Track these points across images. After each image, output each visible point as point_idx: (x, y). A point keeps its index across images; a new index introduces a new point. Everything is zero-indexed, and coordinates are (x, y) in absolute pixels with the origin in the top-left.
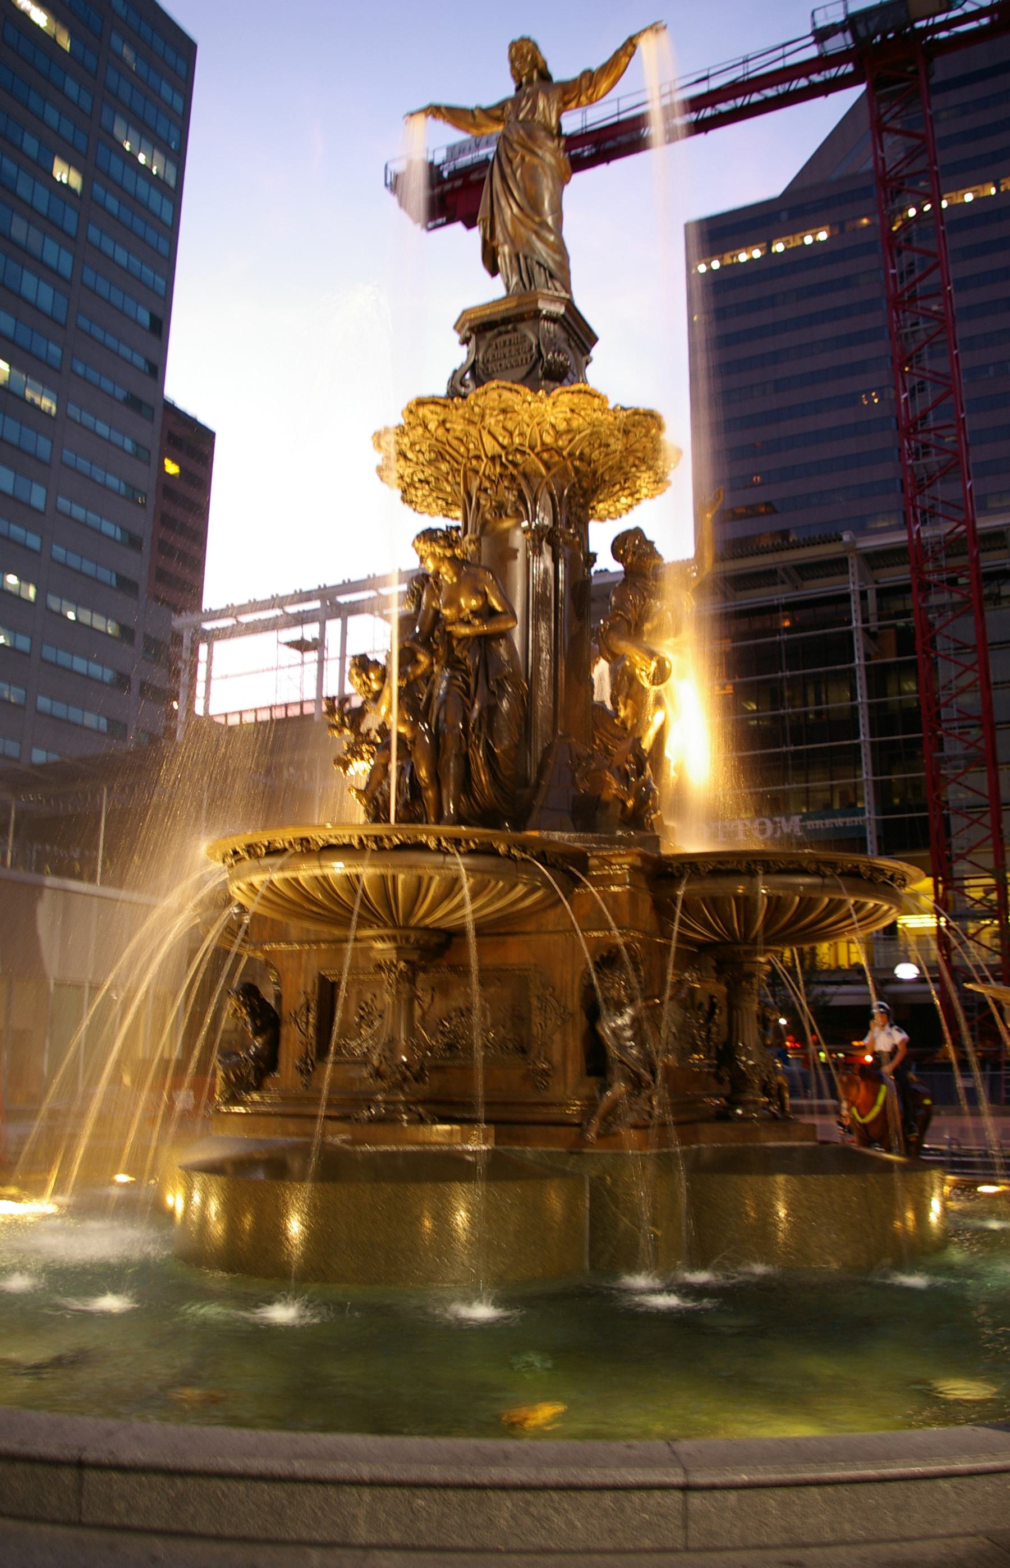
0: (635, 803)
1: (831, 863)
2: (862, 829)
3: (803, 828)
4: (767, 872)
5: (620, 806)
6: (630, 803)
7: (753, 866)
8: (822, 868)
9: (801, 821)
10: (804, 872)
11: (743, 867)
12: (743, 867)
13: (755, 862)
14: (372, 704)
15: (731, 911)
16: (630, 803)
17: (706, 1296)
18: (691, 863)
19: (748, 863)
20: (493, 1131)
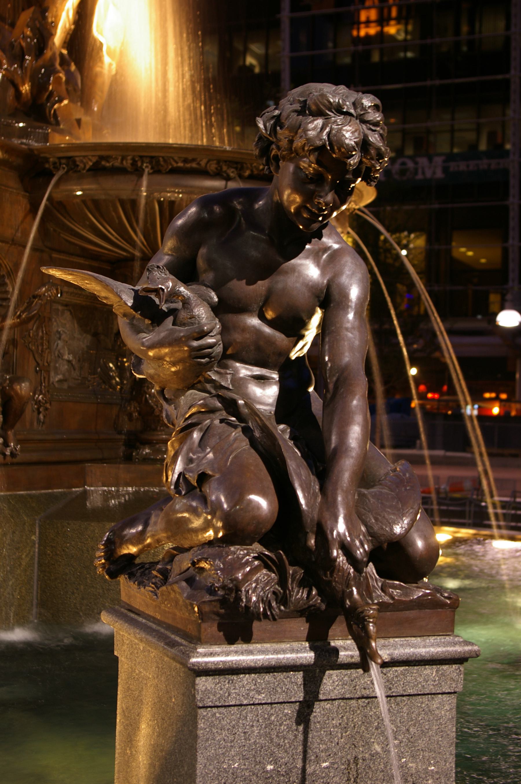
0: (32, 87)
1: (237, 163)
2: (506, 172)
3: (445, 170)
4: (156, 171)
5: (11, 91)
6: (26, 88)
7: (139, 164)
8: (225, 168)
9: (444, 161)
10: (204, 173)
11: (127, 164)
12: (127, 164)
13: (141, 157)
14: (355, 119)
15: (119, 218)
16: (26, 88)
17: (271, 605)
18: (69, 158)
19: (133, 159)
20: (289, 430)
